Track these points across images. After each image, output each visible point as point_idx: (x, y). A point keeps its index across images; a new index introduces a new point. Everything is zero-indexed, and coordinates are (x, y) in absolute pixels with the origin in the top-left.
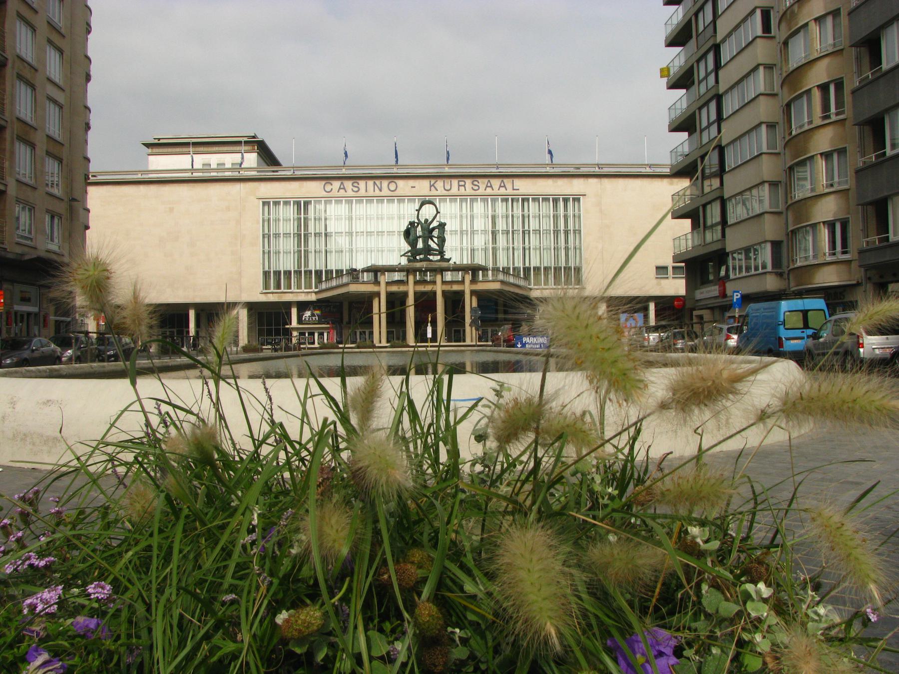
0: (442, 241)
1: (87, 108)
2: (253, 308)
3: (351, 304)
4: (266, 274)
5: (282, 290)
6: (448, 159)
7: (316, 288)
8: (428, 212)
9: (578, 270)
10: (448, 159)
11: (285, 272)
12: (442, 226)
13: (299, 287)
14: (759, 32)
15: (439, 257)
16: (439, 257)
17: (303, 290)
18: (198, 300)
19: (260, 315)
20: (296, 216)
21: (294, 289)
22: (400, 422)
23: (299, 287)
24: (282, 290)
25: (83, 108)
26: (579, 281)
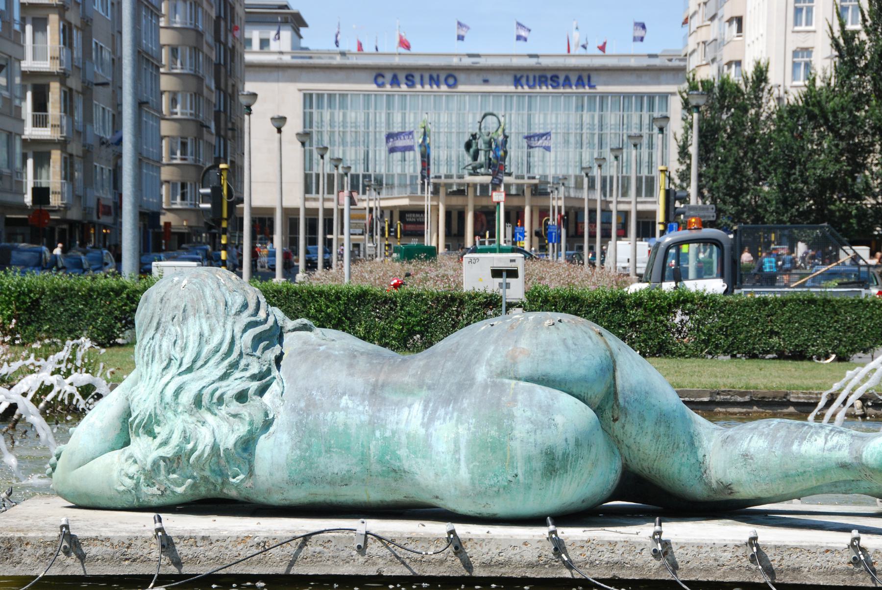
10: (569, 51)
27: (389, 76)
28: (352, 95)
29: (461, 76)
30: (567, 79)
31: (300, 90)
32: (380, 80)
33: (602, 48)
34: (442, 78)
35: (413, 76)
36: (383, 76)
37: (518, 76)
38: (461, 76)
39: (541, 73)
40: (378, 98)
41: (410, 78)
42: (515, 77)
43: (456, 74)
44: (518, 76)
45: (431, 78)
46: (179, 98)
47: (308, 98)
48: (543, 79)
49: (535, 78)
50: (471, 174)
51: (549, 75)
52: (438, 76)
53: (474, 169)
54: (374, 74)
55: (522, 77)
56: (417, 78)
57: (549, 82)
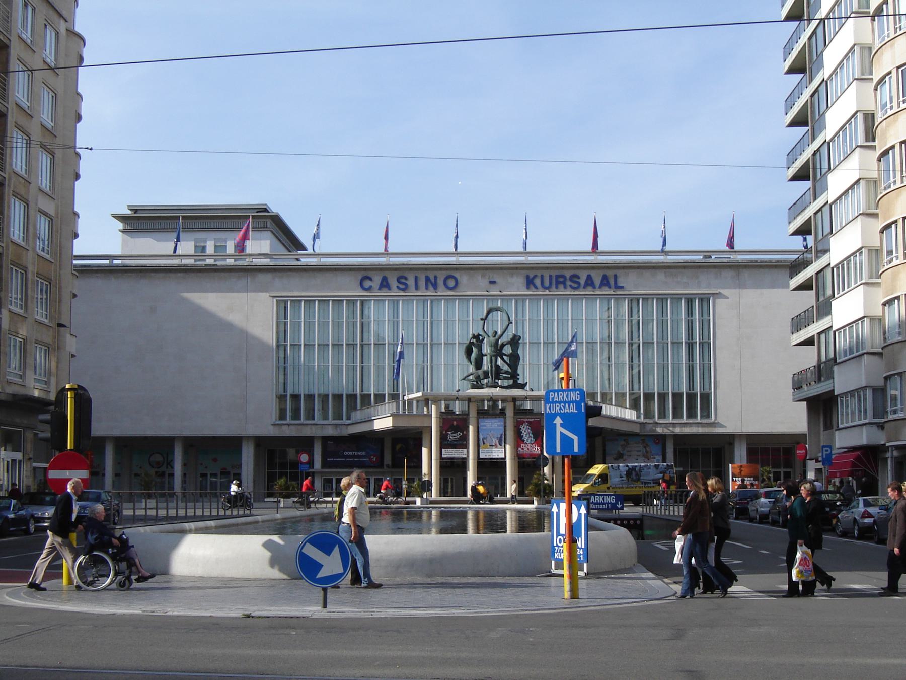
0: (515, 359)
1: (76, 215)
2: (260, 442)
3: (395, 442)
4: (282, 398)
5: (302, 421)
6: (664, 244)
7: (349, 418)
8: (498, 322)
9: (706, 398)
10: (664, 244)
11: (334, 396)
12: (515, 341)
13: (325, 417)
14: (861, 140)
15: (511, 382)
16: (511, 382)
17: (331, 421)
18: (117, 432)
19: (271, 454)
20: (421, 318)
21: (318, 419)
22: (105, 589)
23: (325, 417)
24: (302, 421)
25: (73, 215)
26: (706, 412)
27: (377, 279)
28: (333, 300)
29: (463, 279)
30: (574, 278)
31: (622, 287)
32: (367, 284)
33: (75, 296)
34: (440, 282)
35: (406, 278)
36: (371, 279)
37: (531, 276)
38: (463, 279)
39: (554, 273)
40: (435, 304)
41: (403, 280)
42: (528, 277)
43: (457, 274)
44: (531, 276)
45: (428, 279)
46: (884, 512)
47: (282, 305)
48: (561, 279)
49: (550, 277)
50: (474, 387)
51: (568, 274)
52: (436, 277)
53: (478, 378)
54: (360, 276)
55: (535, 276)
56: (411, 282)
57: (569, 283)
